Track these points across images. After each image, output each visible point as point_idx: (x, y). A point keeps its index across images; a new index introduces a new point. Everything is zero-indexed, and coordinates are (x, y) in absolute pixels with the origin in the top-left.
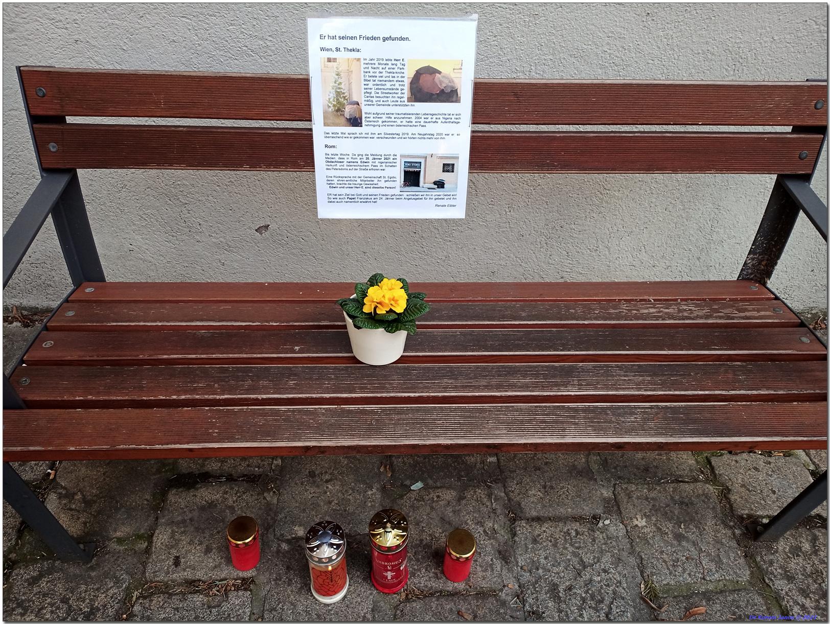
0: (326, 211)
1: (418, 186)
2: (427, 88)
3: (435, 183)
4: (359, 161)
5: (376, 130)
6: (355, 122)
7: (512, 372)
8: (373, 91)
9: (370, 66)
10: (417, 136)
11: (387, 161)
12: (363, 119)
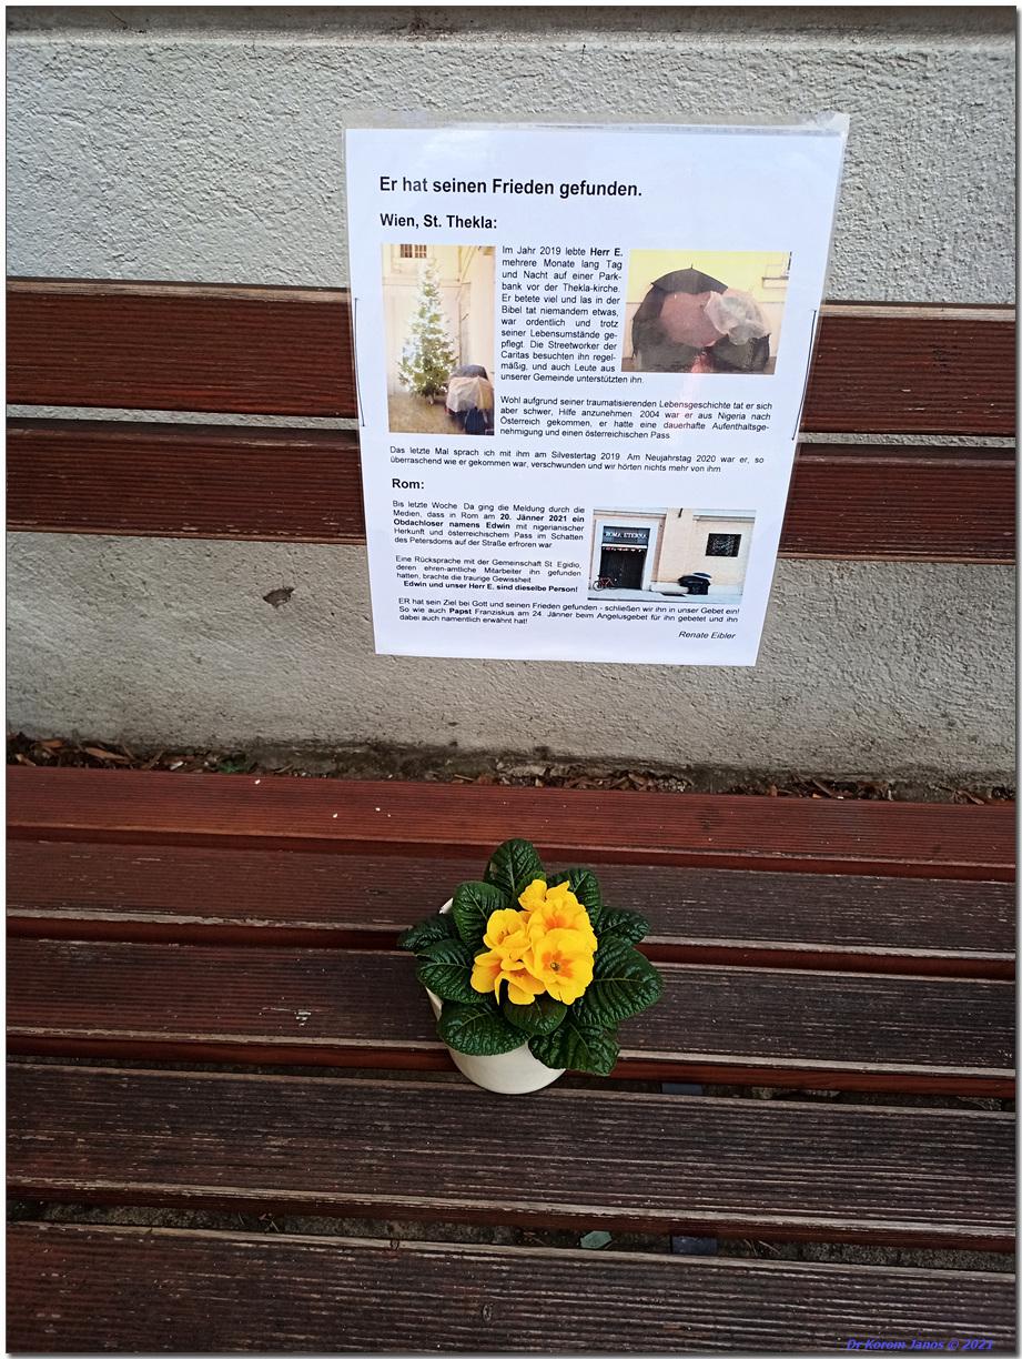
0: (393, 638)
1: (637, 585)
2: (678, 330)
3: (683, 581)
4: (483, 523)
5: (532, 444)
6: (475, 421)
7: (875, 1140)
8: (526, 339)
9: (520, 269)
10: (643, 462)
11: (559, 522)
12: (498, 416)
